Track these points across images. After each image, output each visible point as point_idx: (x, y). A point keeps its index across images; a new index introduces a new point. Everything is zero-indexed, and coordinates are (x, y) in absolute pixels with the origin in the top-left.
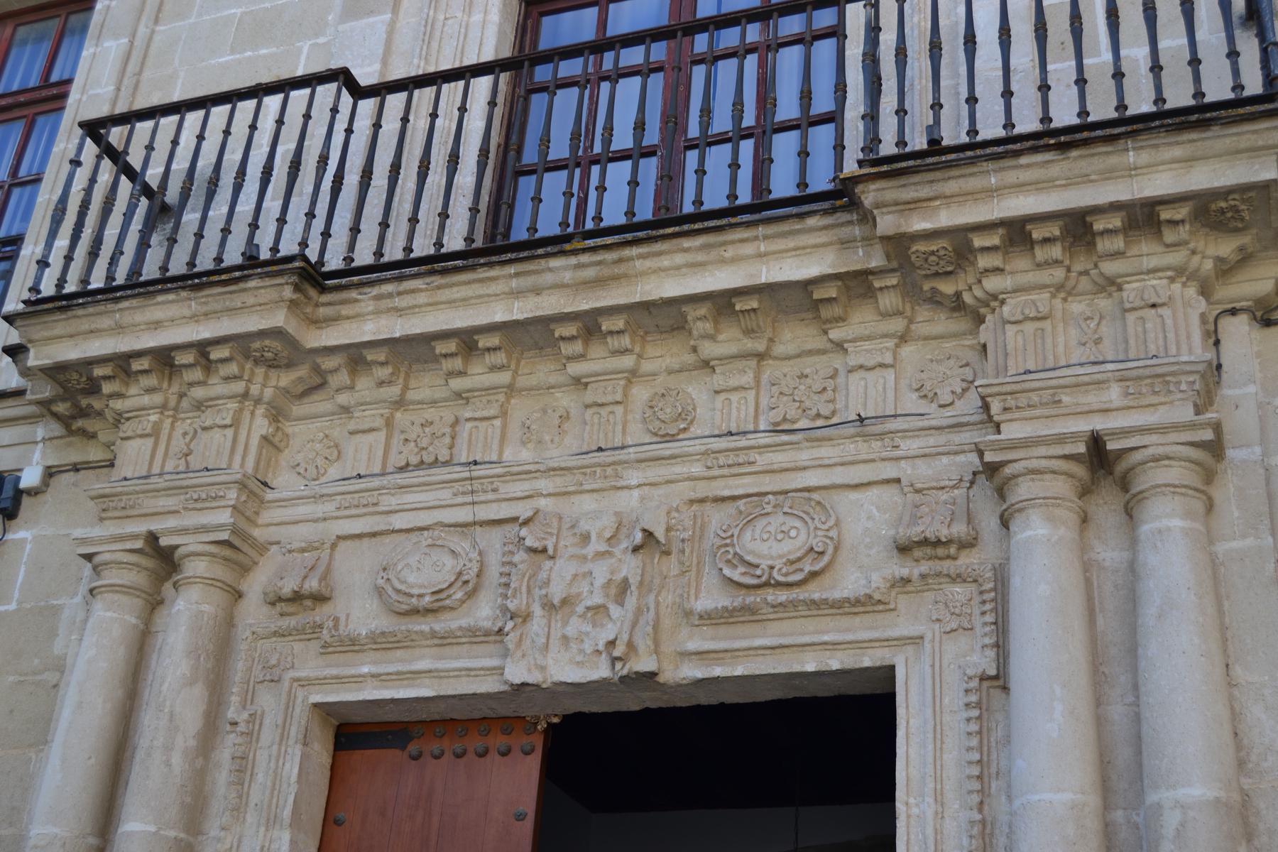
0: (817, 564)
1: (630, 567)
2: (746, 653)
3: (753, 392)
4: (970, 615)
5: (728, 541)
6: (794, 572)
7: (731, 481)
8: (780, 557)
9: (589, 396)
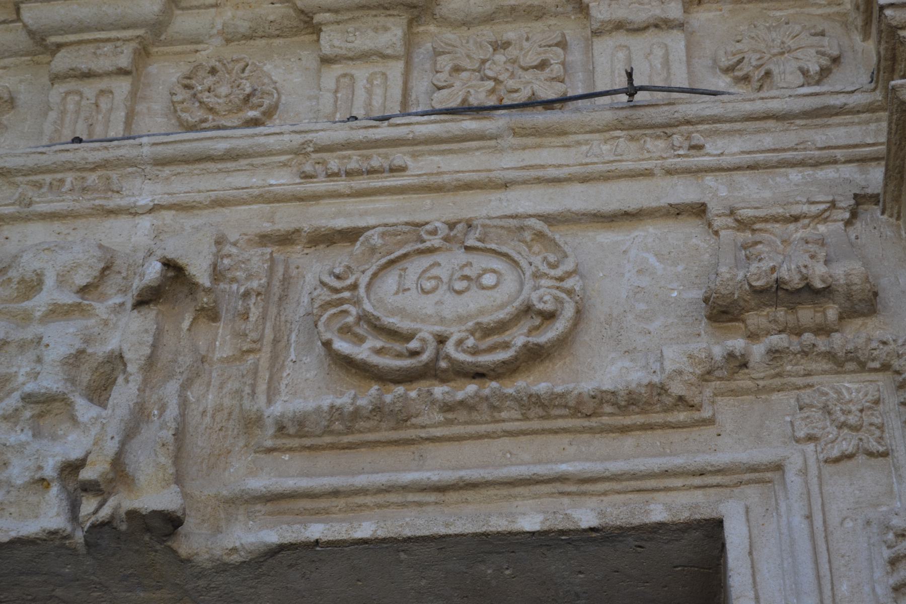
0: (536, 340)
1: (129, 333)
2: (380, 499)
3: (400, 65)
4: (881, 428)
5: (346, 294)
6: (491, 349)
7: (351, 204)
8: (461, 319)
9: (63, 61)
